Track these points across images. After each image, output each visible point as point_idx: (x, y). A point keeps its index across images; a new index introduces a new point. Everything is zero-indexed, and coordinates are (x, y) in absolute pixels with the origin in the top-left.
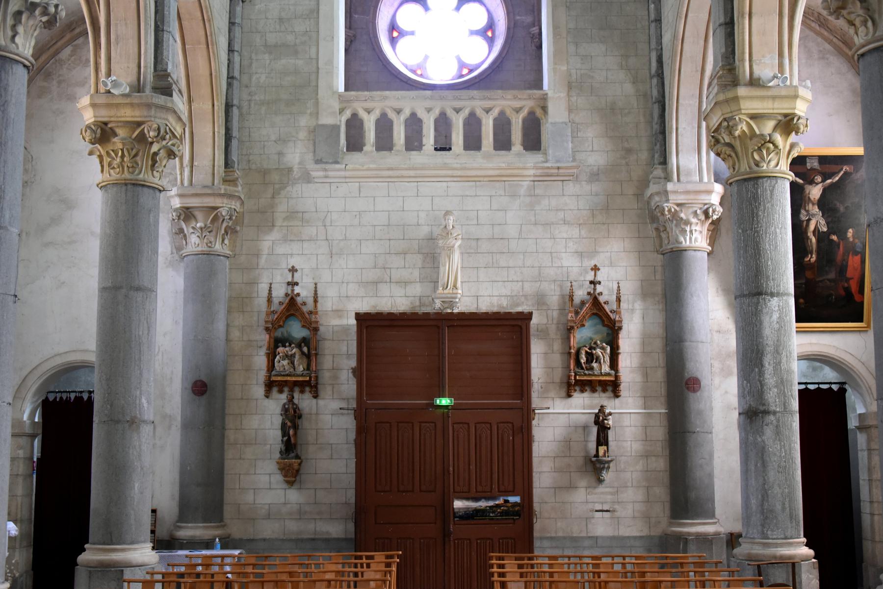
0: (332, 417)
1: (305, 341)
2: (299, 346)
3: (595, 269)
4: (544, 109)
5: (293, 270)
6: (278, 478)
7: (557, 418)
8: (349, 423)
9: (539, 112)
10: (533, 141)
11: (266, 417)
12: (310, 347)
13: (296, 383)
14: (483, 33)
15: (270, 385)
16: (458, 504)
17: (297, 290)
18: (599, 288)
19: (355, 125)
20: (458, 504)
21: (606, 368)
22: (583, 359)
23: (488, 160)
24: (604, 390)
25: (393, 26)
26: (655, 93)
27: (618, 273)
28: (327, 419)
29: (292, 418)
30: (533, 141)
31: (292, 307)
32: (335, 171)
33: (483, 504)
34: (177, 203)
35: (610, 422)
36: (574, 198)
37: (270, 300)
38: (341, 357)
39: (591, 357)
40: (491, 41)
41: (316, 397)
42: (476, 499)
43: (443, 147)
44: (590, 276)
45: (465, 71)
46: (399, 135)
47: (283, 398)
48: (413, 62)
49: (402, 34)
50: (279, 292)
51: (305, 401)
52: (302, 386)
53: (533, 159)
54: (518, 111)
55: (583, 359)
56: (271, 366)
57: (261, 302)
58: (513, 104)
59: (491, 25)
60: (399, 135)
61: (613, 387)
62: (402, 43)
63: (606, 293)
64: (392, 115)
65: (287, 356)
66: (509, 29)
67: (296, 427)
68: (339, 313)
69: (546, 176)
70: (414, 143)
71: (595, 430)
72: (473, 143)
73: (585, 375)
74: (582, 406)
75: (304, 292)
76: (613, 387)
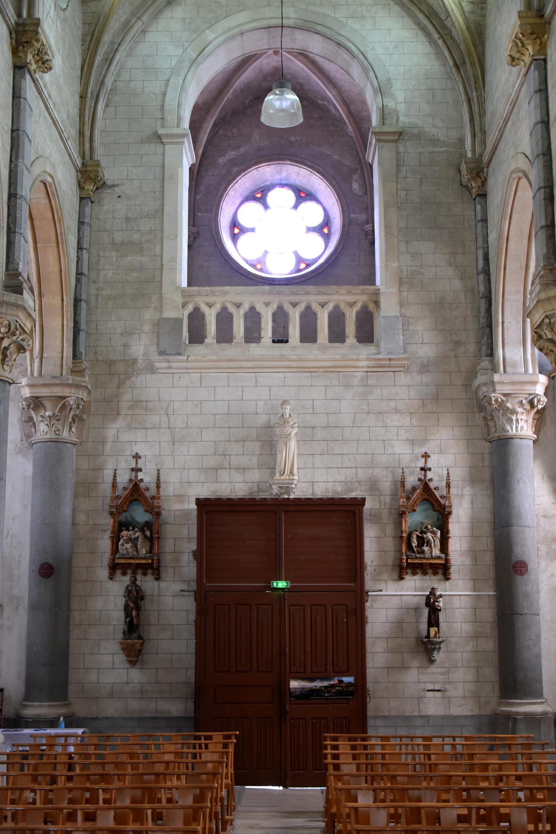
0: (173, 599)
1: (148, 525)
2: (142, 530)
3: (426, 456)
4: (377, 303)
5: (137, 457)
6: (121, 657)
7: (389, 599)
8: (189, 604)
9: (371, 307)
10: (366, 335)
11: (109, 598)
12: (152, 531)
13: (139, 564)
14: (319, 230)
15: (114, 568)
16: (294, 684)
17: (141, 475)
18: (430, 475)
19: (197, 319)
20: (294, 684)
21: (436, 552)
22: (415, 543)
23: (323, 352)
24: (435, 573)
25: (234, 224)
26: (482, 288)
27: (447, 460)
28: (168, 601)
29: (135, 600)
30: (366, 335)
31: (135, 492)
32: (178, 362)
33: (318, 684)
34: (26, 393)
35: (441, 604)
36: (406, 388)
37: (114, 485)
38: (182, 541)
39: (422, 541)
40: (327, 238)
41: (158, 578)
42: (312, 680)
43: (281, 339)
44: (421, 463)
45: (303, 266)
46: (239, 327)
47: (127, 579)
48: (253, 256)
49: (243, 230)
50: (124, 478)
51: (147, 583)
52: (145, 568)
53: (365, 351)
54: (352, 305)
55: (415, 543)
56: (115, 550)
57: (106, 488)
58: (347, 298)
59: (327, 223)
60: (239, 327)
61: (443, 569)
62: (243, 240)
63: (436, 479)
64: (232, 309)
65: (130, 540)
66: (344, 226)
67: (138, 608)
68: (180, 498)
69: (379, 368)
70: (252, 335)
71: (426, 611)
72: (309, 335)
73: (417, 558)
74: (413, 588)
75: (147, 478)
76: (443, 569)
